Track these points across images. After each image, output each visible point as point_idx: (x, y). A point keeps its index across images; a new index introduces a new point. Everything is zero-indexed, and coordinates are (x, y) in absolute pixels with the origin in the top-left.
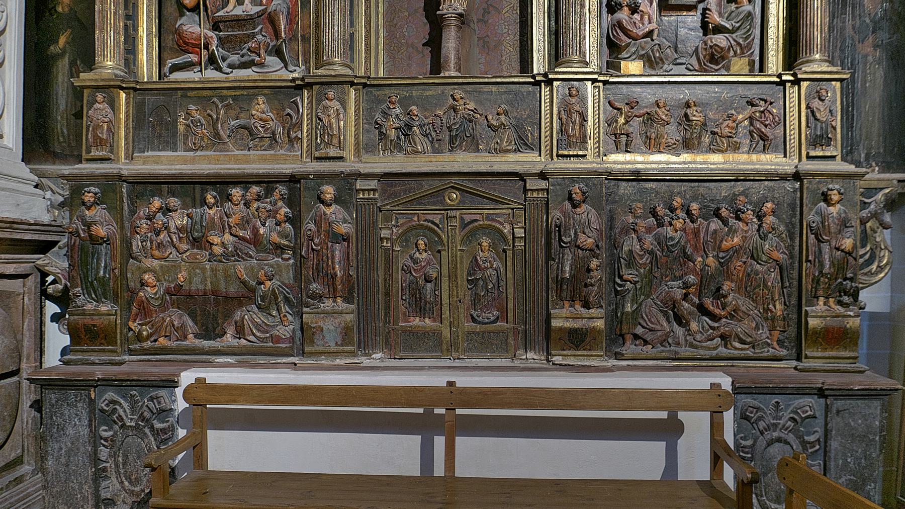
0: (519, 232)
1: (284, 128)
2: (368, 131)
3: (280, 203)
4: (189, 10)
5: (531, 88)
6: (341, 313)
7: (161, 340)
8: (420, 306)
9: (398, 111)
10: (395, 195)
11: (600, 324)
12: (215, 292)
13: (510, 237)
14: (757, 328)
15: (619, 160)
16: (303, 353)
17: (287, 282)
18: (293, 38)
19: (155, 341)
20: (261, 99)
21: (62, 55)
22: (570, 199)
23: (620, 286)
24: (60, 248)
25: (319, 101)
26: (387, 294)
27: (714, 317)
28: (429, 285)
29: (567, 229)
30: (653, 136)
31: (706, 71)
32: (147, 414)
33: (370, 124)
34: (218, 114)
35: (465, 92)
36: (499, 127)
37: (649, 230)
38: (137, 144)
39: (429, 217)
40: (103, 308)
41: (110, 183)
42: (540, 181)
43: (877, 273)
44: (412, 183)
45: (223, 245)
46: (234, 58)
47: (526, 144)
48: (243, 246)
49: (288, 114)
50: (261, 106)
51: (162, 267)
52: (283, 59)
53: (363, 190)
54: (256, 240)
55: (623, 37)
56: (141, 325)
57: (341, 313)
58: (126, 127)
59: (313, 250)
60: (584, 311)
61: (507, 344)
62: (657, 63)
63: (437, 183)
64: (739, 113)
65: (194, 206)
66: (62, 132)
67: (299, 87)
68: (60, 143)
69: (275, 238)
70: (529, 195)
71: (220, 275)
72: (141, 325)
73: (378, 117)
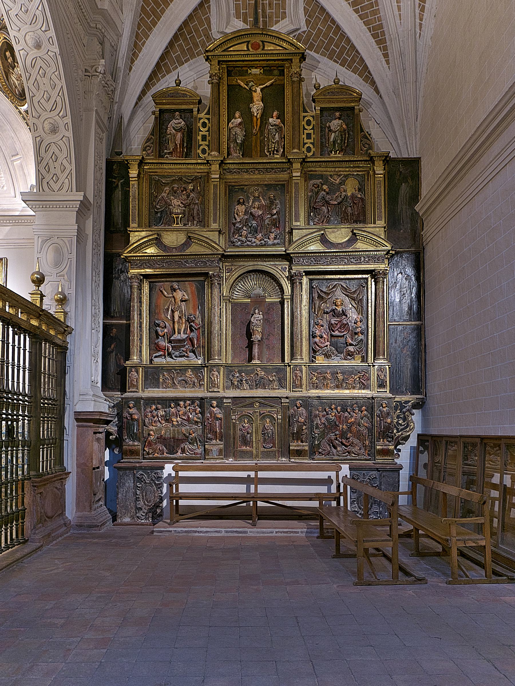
0: (280, 417)
1: (197, 380)
2: (227, 382)
3: (197, 407)
4: (161, 336)
5: (283, 367)
6: (219, 445)
7: (156, 454)
8: (245, 442)
9: (238, 375)
10: (237, 404)
11: (307, 448)
12: (173, 438)
13: (276, 419)
14: (360, 449)
15: (314, 393)
16: (205, 458)
17: (199, 434)
18: (199, 346)
19: (154, 455)
20: (189, 370)
21: (112, 352)
22: (296, 406)
23: (314, 435)
24: (113, 422)
25: (211, 372)
26: (234, 438)
27: (346, 446)
28: (248, 435)
29: (295, 416)
30: (325, 384)
31: (346, 360)
32: (154, 479)
33: (228, 379)
34: (174, 376)
35: (261, 368)
36: (273, 380)
37: (323, 416)
38: (146, 386)
39: (248, 412)
40: (136, 443)
41: (137, 400)
42: (286, 400)
43: (409, 431)
44: (243, 400)
45: (177, 421)
46: (177, 353)
47: (282, 386)
48: (184, 422)
49: (199, 376)
50: (189, 373)
51: (156, 429)
52: (195, 355)
53: (226, 403)
54: (188, 420)
55: (317, 347)
56: (149, 449)
57: (219, 445)
58: (142, 380)
59: (209, 423)
60: (301, 443)
61: (276, 455)
62: (329, 357)
63: (251, 400)
64: (355, 376)
65: (166, 408)
66: (112, 380)
67: (202, 367)
68: (111, 384)
69: (196, 419)
70: (283, 404)
71: (176, 432)
72: (149, 449)
73: (231, 377)
